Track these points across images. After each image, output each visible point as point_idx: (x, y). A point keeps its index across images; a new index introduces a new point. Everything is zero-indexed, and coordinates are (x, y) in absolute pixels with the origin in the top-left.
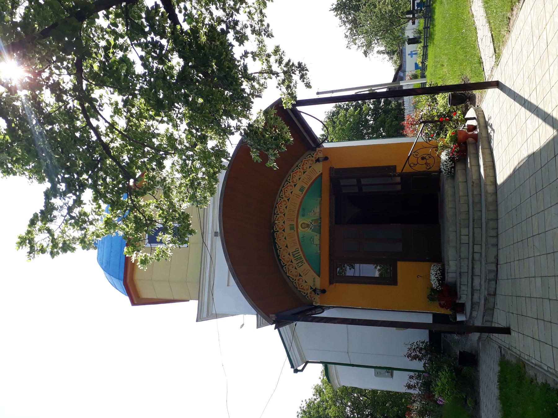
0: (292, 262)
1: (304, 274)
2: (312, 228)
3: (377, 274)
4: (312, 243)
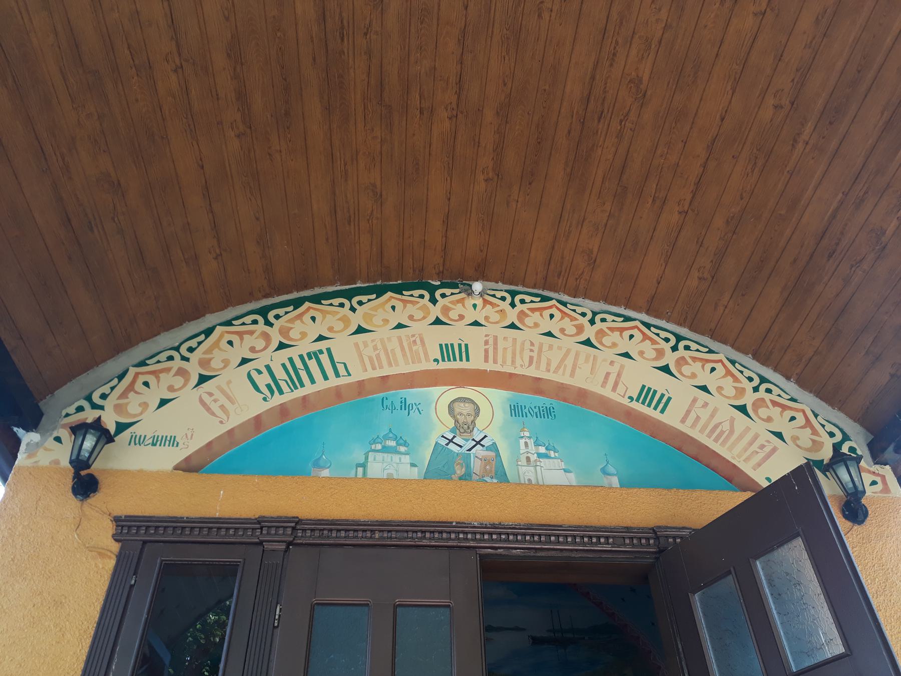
0: (282, 346)
1: (211, 394)
2: (451, 446)
3: (652, 327)
4: (374, 442)
